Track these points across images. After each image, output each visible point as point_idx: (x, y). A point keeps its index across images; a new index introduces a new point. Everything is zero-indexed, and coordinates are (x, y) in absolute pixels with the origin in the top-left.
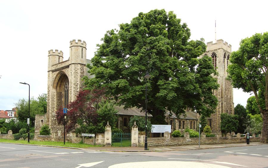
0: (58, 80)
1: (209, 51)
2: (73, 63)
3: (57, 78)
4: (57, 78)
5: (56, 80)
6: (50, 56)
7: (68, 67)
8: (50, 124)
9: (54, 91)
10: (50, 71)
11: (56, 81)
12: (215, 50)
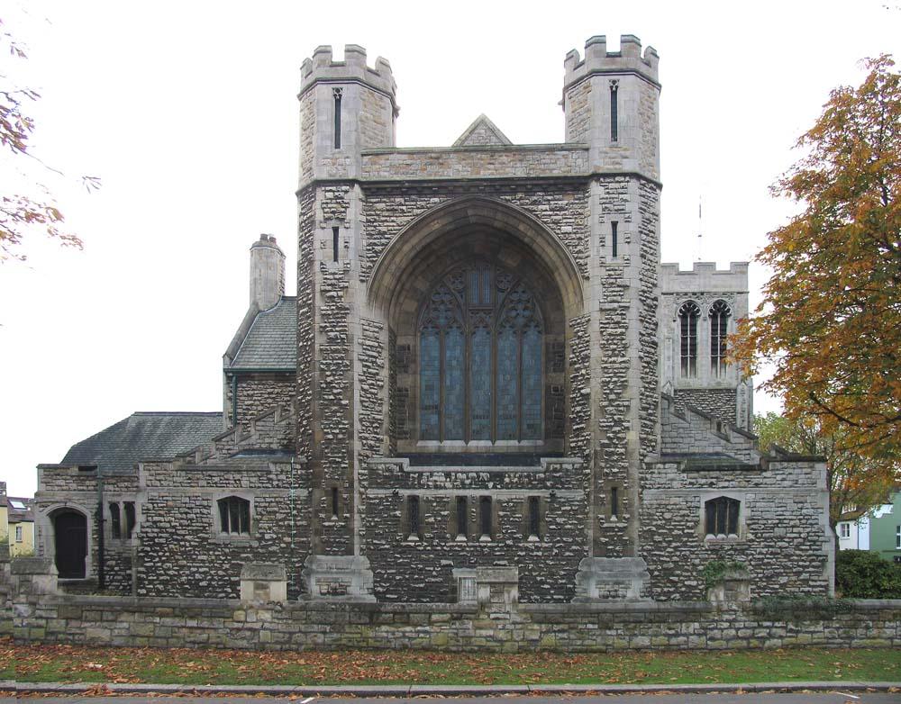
0: (413, 254)
1: (702, 294)
2: (628, 166)
3: (414, 241)
4: (414, 241)
5: (406, 248)
6: (348, 91)
7: (577, 185)
8: (357, 524)
9: (376, 316)
10: (351, 182)
11: (397, 260)
12: (694, 294)
